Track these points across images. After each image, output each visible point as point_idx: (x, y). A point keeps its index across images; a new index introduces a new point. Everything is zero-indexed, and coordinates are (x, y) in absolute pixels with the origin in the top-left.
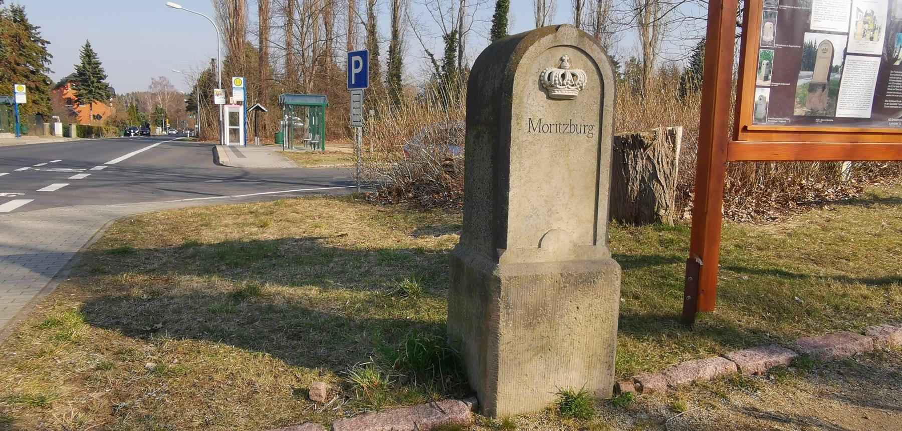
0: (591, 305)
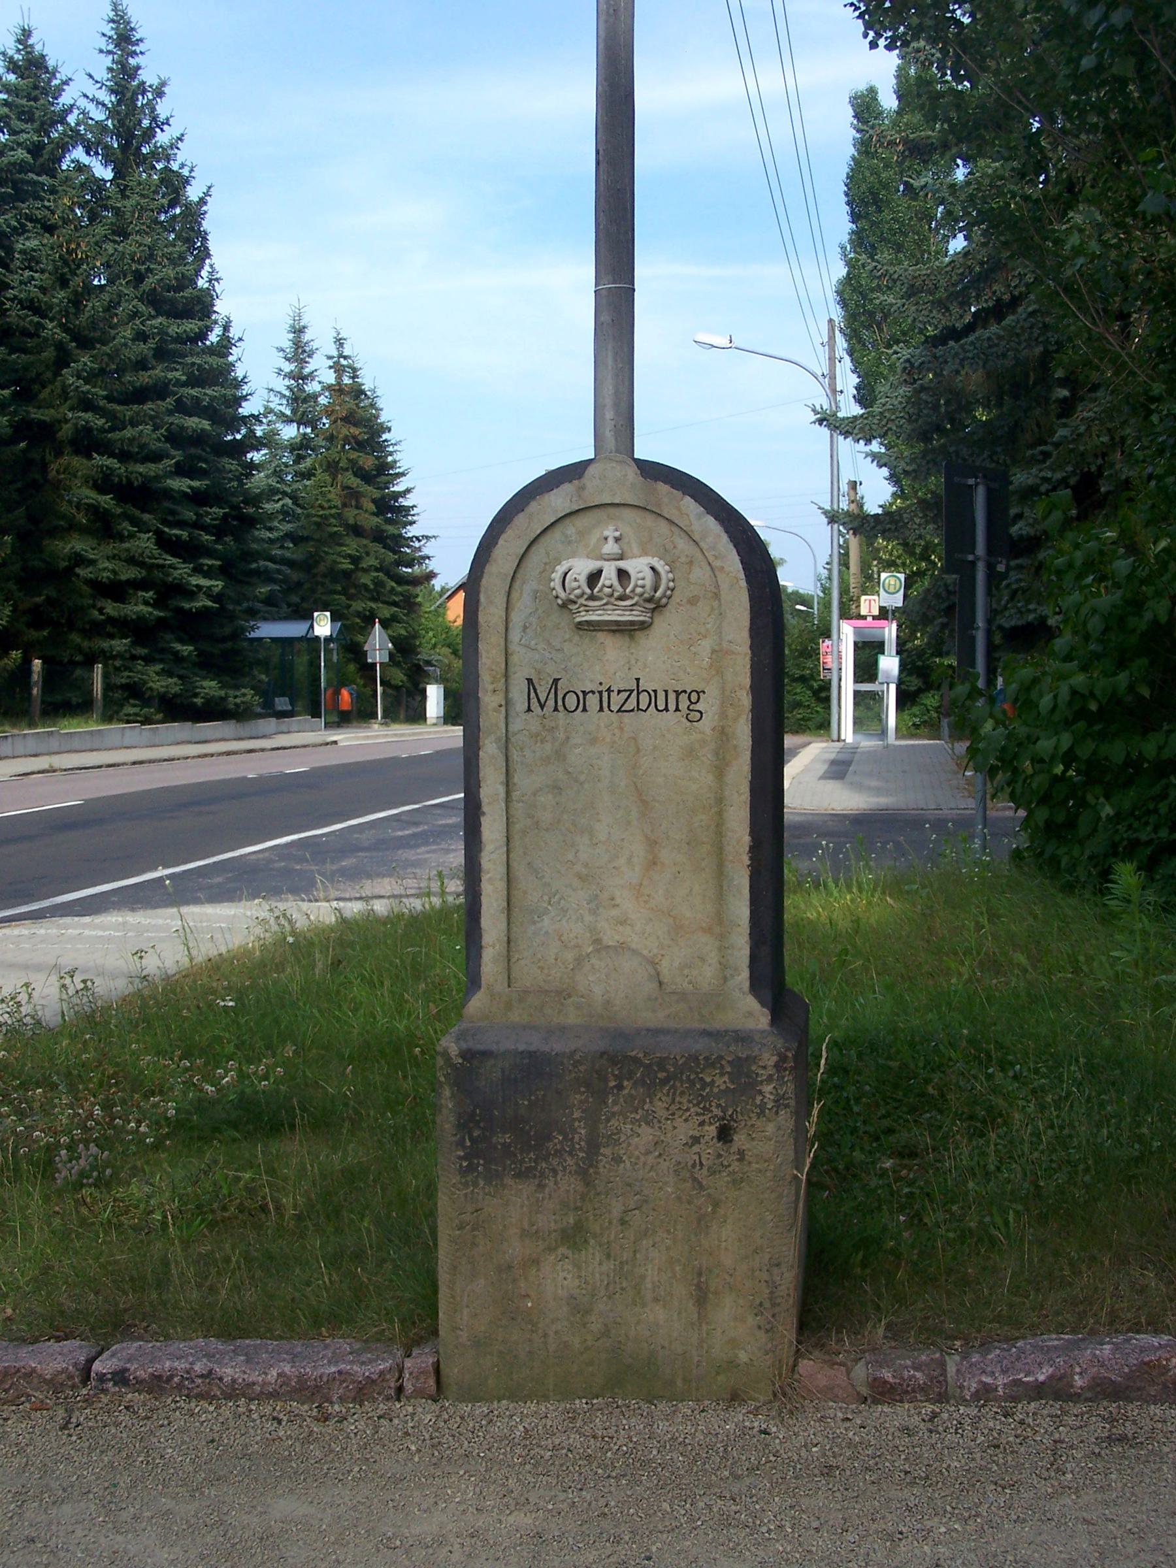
0: (696, 1140)
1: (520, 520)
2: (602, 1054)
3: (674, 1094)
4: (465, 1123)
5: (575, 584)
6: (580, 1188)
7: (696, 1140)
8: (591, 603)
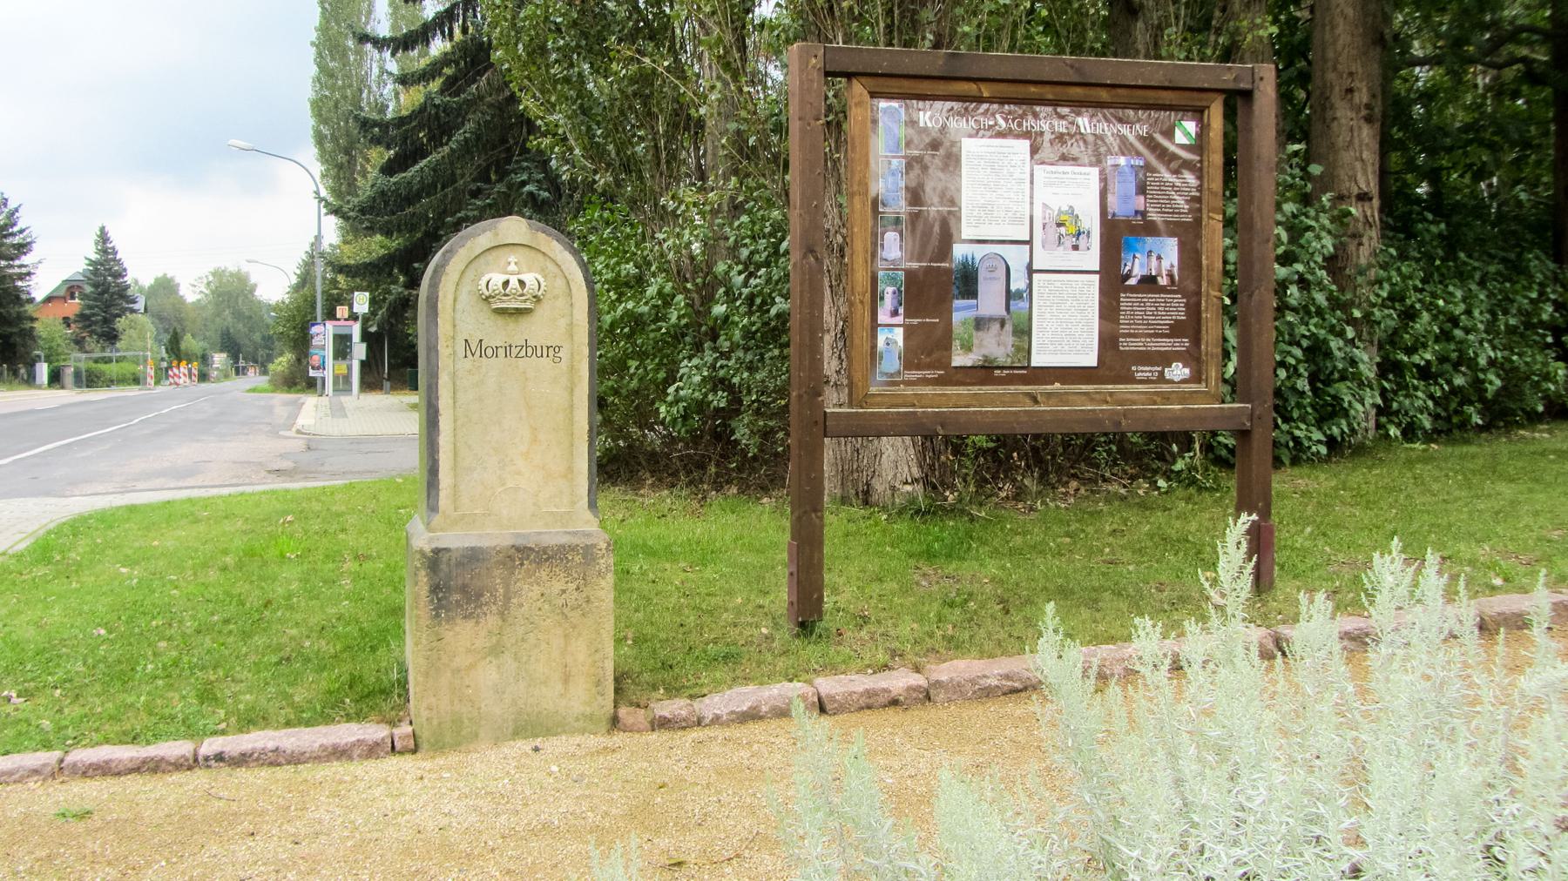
0: (564, 591)
7: (564, 591)
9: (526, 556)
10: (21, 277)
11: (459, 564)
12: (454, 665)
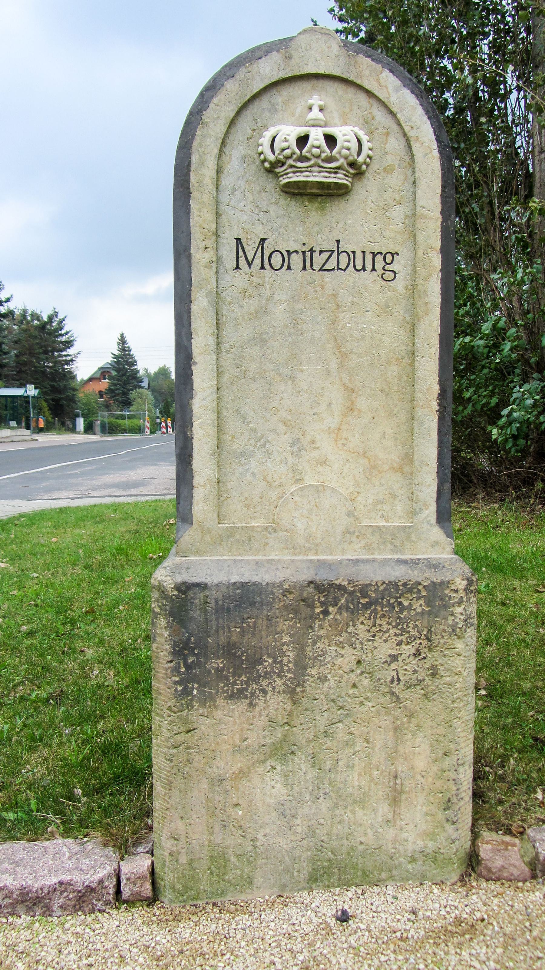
0: (394, 658)
1: (230, 86)
2: (311, 582)
3: (375, 618)
4: (180, 650)
5: (285, 145)
6: (289, 706)
7: (394, 658)
8: (299, 164)
9: (333, 599)
10: (67, 362)
11: (221, 610)
12: (214, 771)
